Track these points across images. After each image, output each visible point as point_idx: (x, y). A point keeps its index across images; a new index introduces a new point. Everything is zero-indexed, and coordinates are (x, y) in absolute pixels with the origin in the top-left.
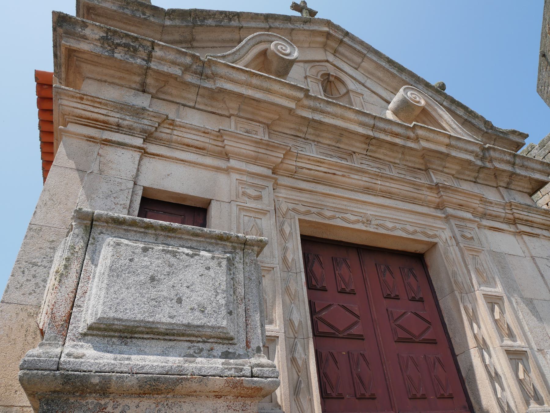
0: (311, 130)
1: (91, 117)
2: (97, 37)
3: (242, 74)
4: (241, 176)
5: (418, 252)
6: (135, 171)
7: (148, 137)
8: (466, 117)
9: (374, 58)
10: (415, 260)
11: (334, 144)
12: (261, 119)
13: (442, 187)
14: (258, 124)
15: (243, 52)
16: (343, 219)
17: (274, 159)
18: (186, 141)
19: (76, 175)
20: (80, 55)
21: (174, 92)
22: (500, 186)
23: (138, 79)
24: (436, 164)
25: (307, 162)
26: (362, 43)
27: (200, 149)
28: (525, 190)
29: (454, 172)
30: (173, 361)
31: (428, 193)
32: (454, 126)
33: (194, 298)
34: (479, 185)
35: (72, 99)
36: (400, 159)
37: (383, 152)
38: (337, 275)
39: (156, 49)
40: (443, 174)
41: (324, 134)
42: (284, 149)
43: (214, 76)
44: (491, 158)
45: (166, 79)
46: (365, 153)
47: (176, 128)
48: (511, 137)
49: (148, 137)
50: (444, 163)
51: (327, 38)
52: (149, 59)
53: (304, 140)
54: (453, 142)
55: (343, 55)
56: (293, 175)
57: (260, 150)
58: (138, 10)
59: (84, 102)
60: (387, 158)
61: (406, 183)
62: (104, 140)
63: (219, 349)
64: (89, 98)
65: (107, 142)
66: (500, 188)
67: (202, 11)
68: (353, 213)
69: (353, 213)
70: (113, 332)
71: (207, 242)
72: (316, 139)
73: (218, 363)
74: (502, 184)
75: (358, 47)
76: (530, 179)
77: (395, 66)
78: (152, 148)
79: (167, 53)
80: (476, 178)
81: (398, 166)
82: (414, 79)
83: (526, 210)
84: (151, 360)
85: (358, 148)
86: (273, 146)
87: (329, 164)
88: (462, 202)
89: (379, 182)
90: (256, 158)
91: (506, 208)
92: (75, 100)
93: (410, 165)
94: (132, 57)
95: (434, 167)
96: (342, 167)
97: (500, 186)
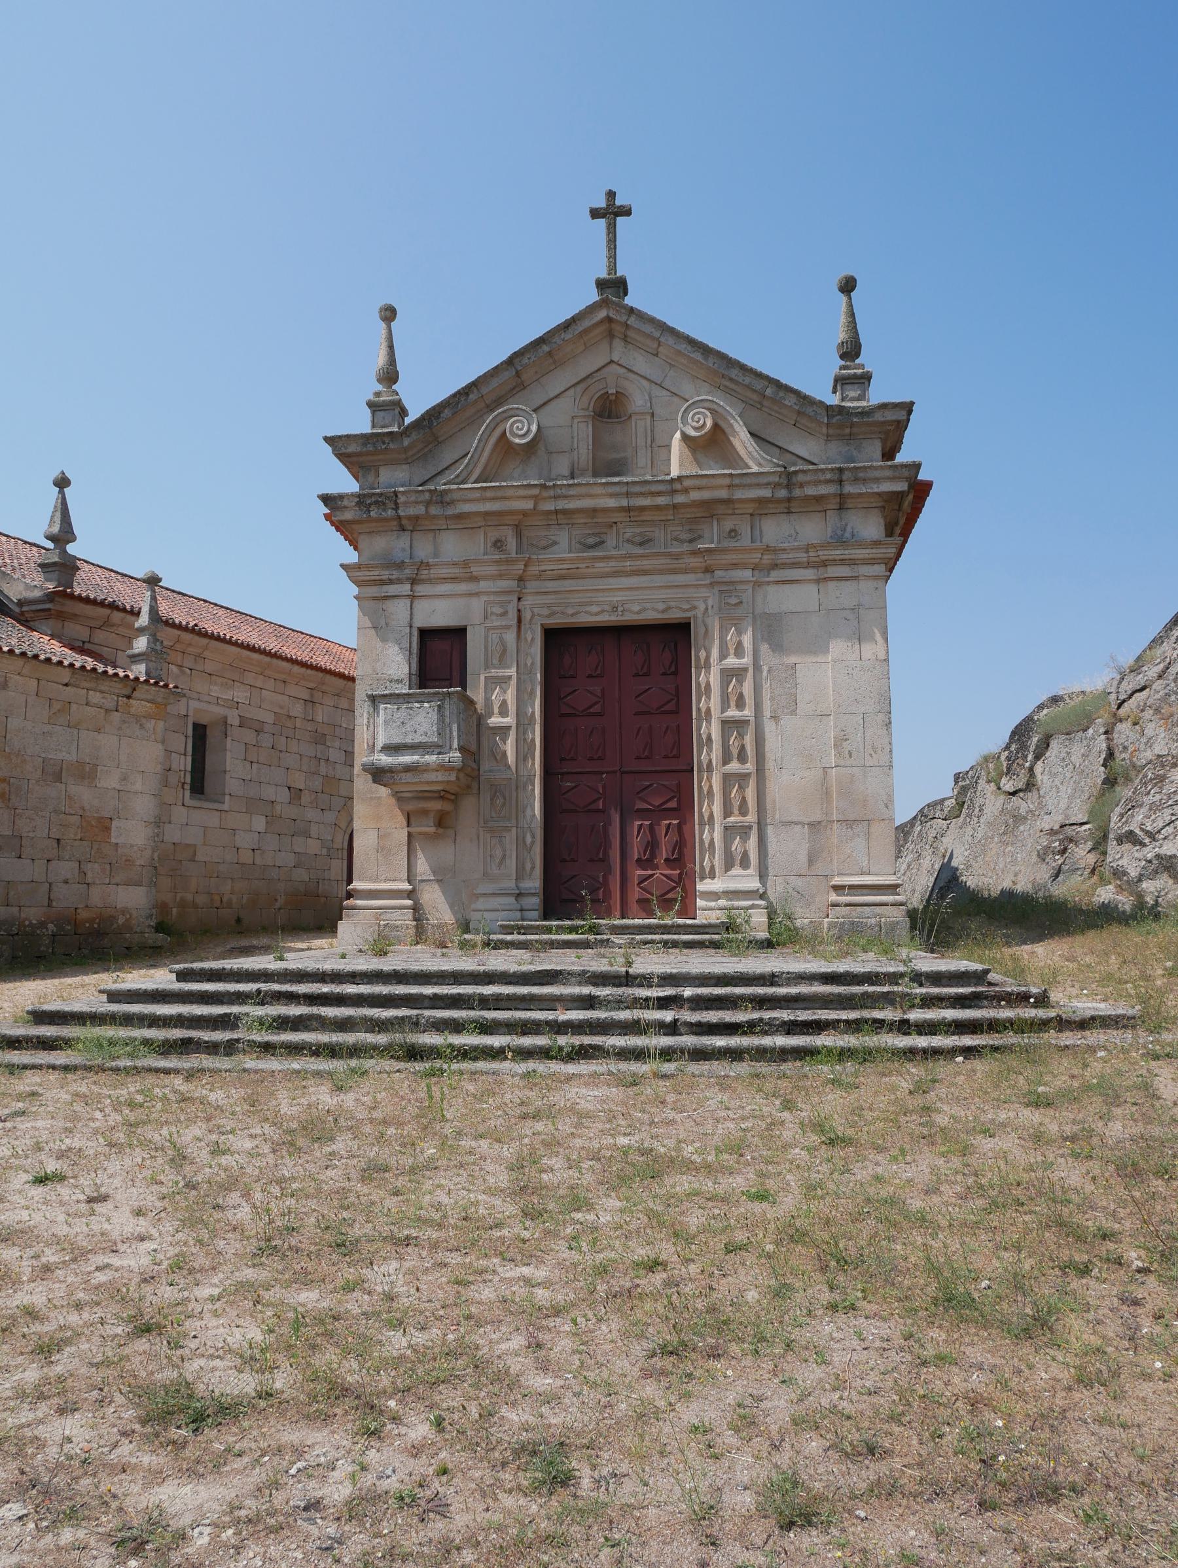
7: (414, 582)
15: (476, 457)
19: (373, 631)
27: (454, 579)
28: (874, 505)
30: (416, 758)
31: (692, 560)
32: (751, 449)
33: (422, 729)
43: (452, 503)
45: (416, 519)
49: (414, 582)
54: (736, 481)
56: (539, 577)
63: (437, 750)
67: (433, 408)
68: (598, 604)
69: (598, 604)
70: (390, 749)
73: (434, 757)
76: (879, 494)
78: (421, 589)
84: (406, 759)
89: (628, 563)
94: (384, 510)
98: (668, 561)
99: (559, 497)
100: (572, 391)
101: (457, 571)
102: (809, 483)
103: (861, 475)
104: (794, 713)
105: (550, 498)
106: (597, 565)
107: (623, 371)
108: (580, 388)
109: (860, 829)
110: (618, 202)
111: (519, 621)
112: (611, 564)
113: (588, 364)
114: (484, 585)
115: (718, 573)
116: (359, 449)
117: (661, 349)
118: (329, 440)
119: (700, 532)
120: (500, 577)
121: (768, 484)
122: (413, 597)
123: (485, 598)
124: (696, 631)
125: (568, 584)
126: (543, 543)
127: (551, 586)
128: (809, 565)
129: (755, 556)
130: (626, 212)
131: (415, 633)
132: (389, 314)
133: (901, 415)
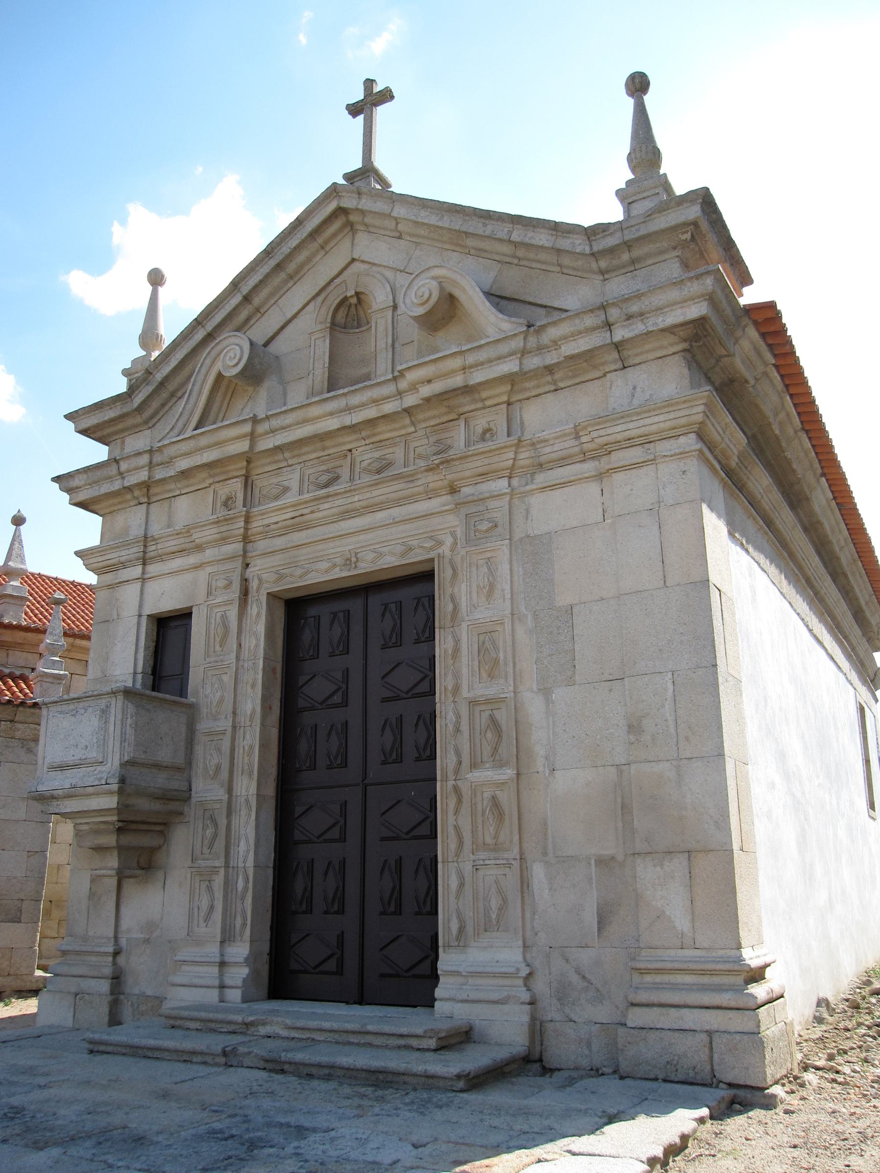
24: (466, 404)
34: (565, 392)
42: (241, 516)
50: (477, 396)
53: (289, 469)
56: (267, 533)
78: (152, 569)
85: (350, 442)
88: (481, 470)
89: (356, 499)
93: (433, 423)
96: (306, 502)
98: (402, 486)
99: (276, 430)
100: (312, 304)
101: (182, 541)
102: (565, 338)
103: (634, 308)
104: (570, 682)
106: (322, 507)
107: (366, 266)
108: (320, 299)
109: (678, 864)
110: (377, 88)
111: (245, 593)
112: (338, 503)
113: (327, 267)
114: (210, 554)
115: (466, 490)
117: (401, 227)
119: (449, 442)
121: (511, 354)
122: (143, 579)
123: (209, 569)
124: (443, 576)
125: (298, 537)
126: (275, 491)
127: (280, 542)
128: (585, 456)
129: (505, 457)
130: (387, 96)
131: (144, 621)
132: (18, 521)
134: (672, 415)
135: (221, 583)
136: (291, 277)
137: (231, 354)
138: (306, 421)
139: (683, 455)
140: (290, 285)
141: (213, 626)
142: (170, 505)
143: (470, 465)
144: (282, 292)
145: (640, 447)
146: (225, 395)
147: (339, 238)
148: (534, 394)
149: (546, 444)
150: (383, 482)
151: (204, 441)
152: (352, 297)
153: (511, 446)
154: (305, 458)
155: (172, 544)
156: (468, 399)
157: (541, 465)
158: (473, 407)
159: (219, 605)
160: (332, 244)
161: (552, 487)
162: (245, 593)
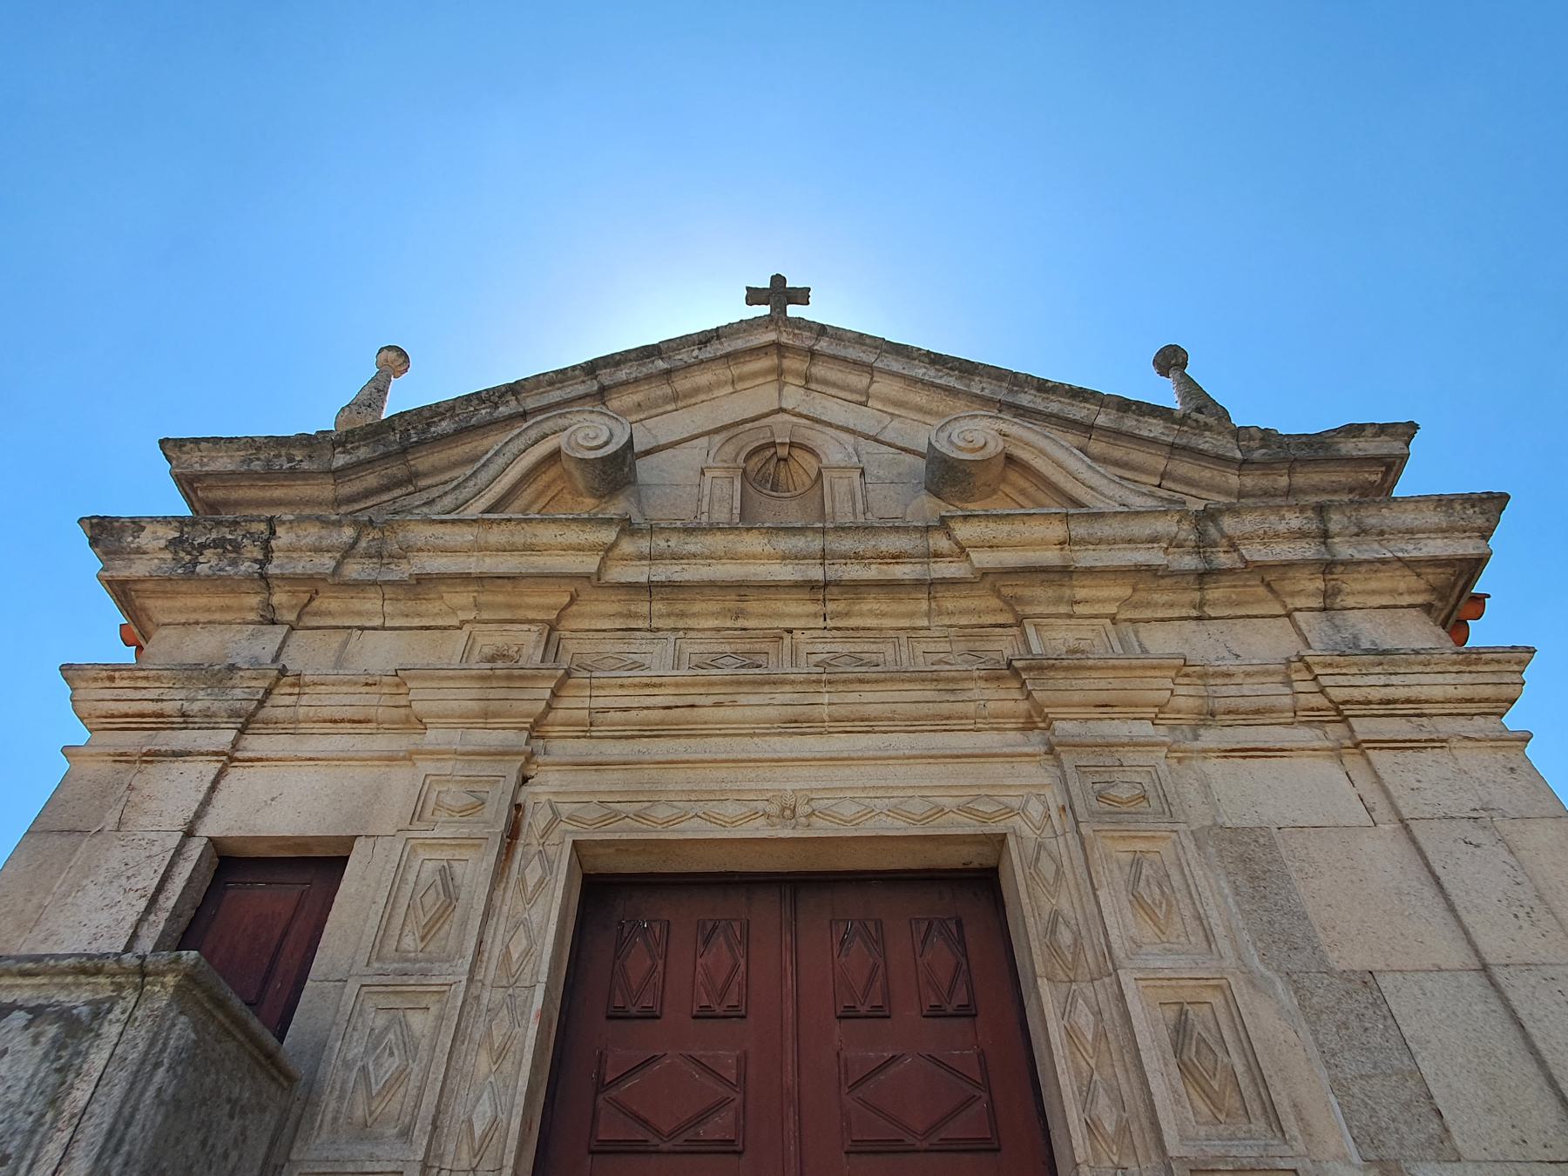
0: (658, 607)
1: (130, 712)
2: (162, 543)
3: (465, 529)
4: (439, 764)
5: (975, 865)
6: (195, 806)
8: (1170, 439)
9: (896, 366)
10: (963, 891)
11: (729, 624)
12: (531, 615)
13: (1028, 669)
14: (526, 627)
16: (708, 818)
17: (526, 706)
18: (326, 713)
20: (138, 587)
21: (334, 605)
22: (1297, 610)
23: (254, 600)
25: (620, 692)
26: (861, 339)
29: (1112, 609)
31: (988, 694)
35: (94, 685)
36: (928, 614)
37: (871, 611)
38: (699, 969)
39: (280, 531)
40: (1074, 621)
41: (697, 607)
42: (551, 677)
44: (1230, 538)
45: (312, 584)
46: (821, 624)
47: (307, 690)
48: (1348, 447)
50: (1067, 592)
51: (781, 356)
52: (266, 556)
53: (648, 635)
55: (825, 382)
56: (587, 729)
57: (493, 694)
58: (278, 456)
59: (118, 683)
60: (888, 622)
61: (910, 681)
62: (145, 755)
64: (125, 674)
65: (152, 756)
66: (1297, 614)
71: (56, 985)
72: (680, 624)
74: (1300, 602)
75: (853, 353)
77: (951, 369)
78: (256, 744)
79: (302, 533)
80: (1201, 605)
81: (926, 633)
82: (1005, 385)
83: (1378, 669)
86: (521, 678)
87: (677, 685)
88: (1104, 697)
89: (826, 698)
90: (486, 715)
91: (1294, 677)
92: (100, 684)
93: (964, 621)
94: (234, 563)
95: (1038, 610)
97: (1297, 610)
100: (704, 441)
105: (641, 557)
106: (742, 699)
111: (513, 832)
116: (231, 467)
118: (169, 446)
120: (486, 717)
121: (1154, 539)
122: (229, 758)
125: (660, 748)
131: (195, 849)
133: (1395, 447)
134: (1466, 678)
135: (455, 796)
136: (675, 398)
137: (590, 433)
138: (733, 557)
139: (1500, 744)
140: (669, 408)
141: (408, 889)
142: (345, 644)
143: (1086, 684)
144: (654, 412)
145: (1403, 720)
146: (540, 495)
147: (757, 382)
148: (1160, 615)
149: (1227, 681)
150: (892, 680)
151: (496, 536)
152: (783, 444)
153: (1169, 668)
154: (691, 623)
155: (335, 702)
156: (1050, 593)
157: (1213, 714)
158: (1052, 610)
159: (439, 844)
160: (747, 384)
161: (1247, 752)
162: (513, 832)
